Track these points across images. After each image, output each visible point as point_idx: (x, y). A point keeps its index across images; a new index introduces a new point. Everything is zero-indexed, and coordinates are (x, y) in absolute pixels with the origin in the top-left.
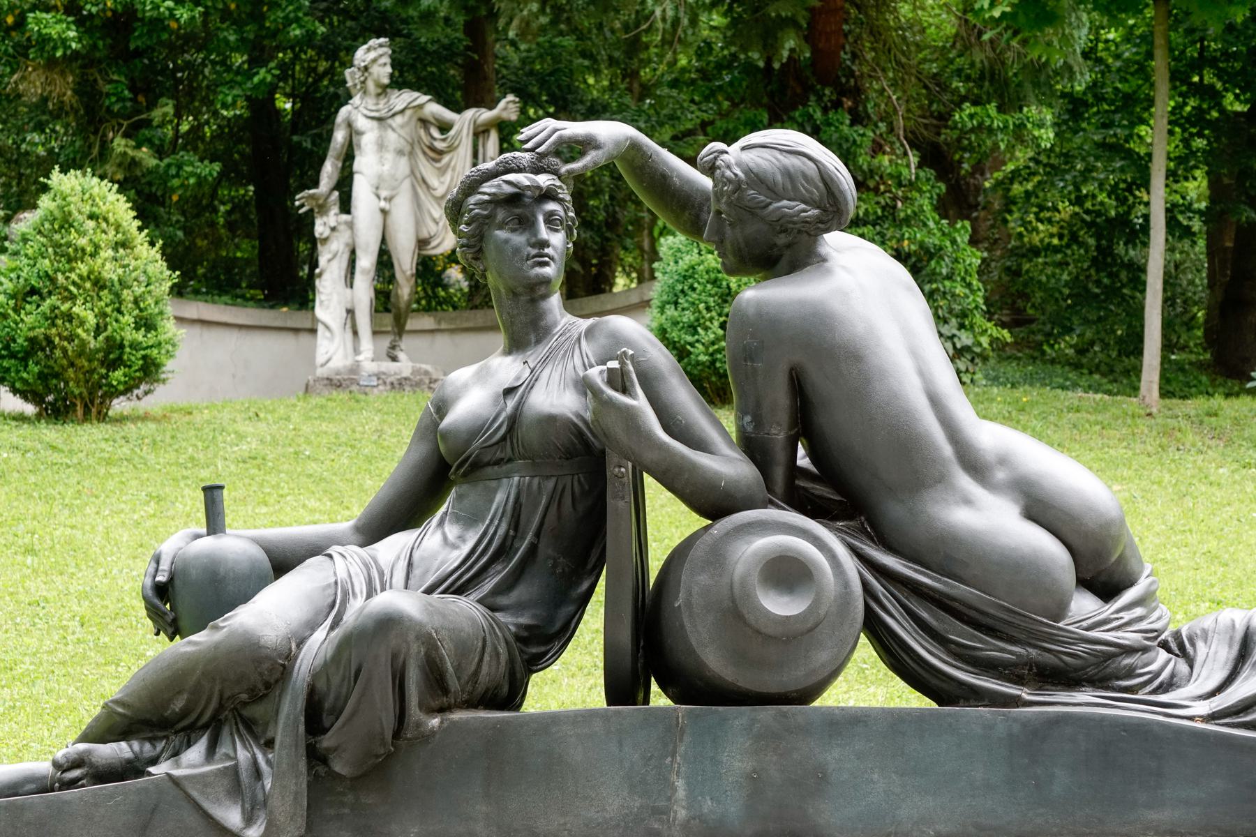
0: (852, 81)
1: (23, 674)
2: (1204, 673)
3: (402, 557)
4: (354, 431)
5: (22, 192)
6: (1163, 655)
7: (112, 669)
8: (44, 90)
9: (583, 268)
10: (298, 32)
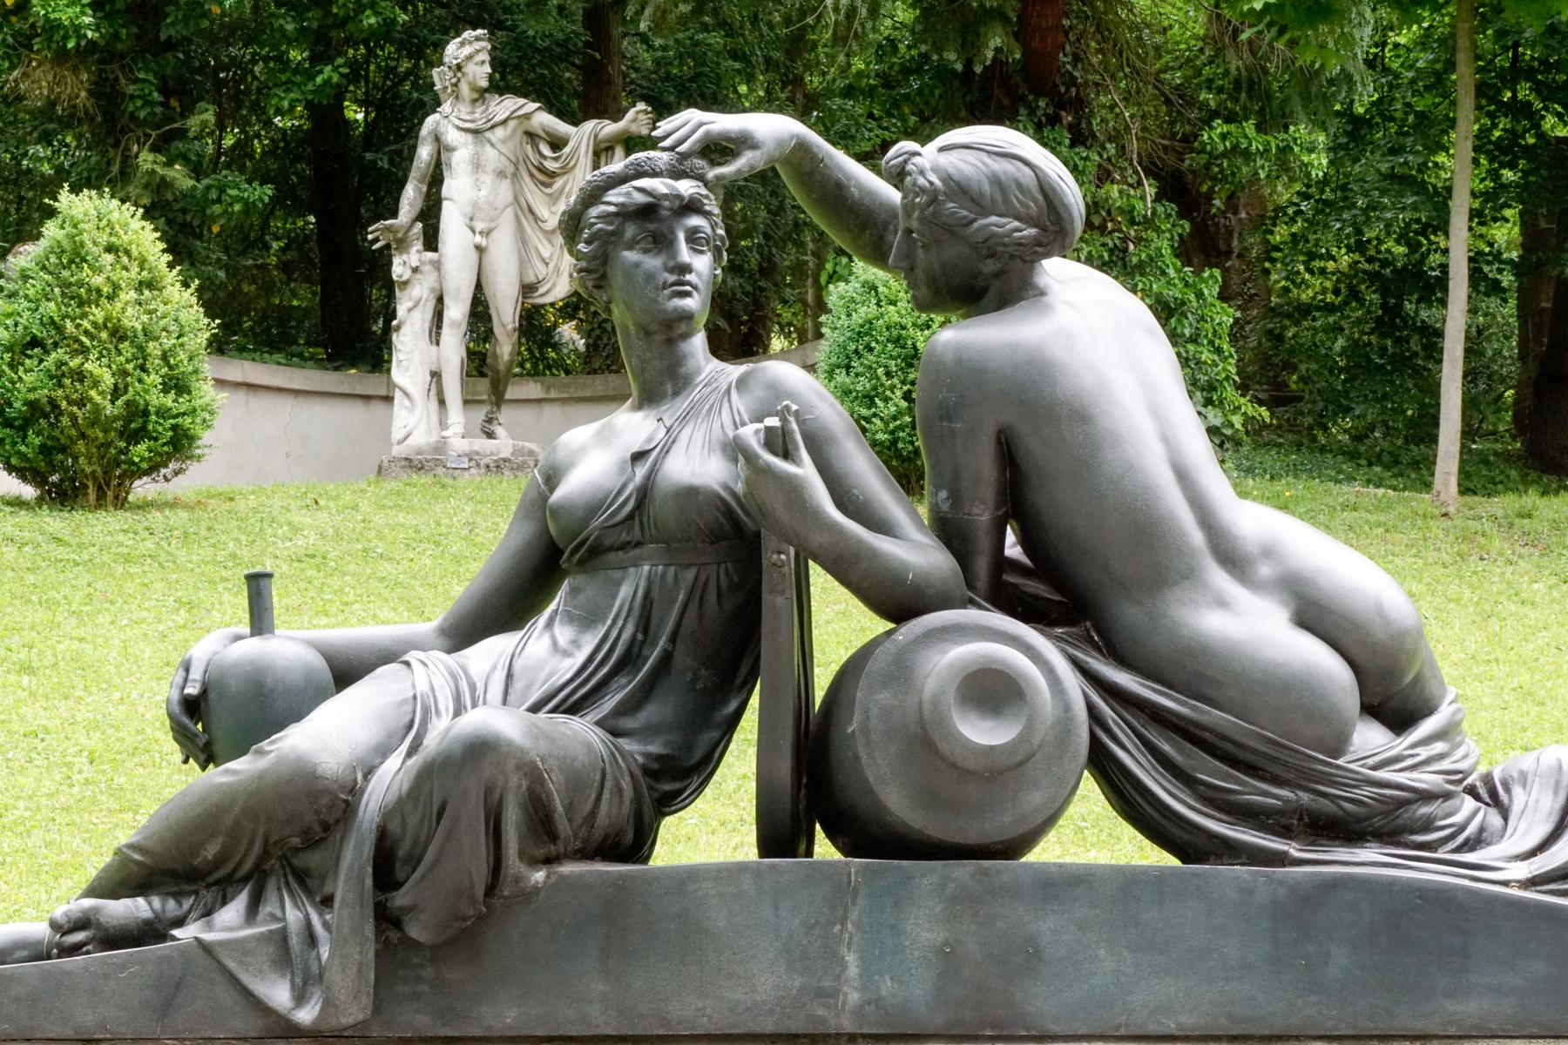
0: (1073, 90)
1: (15, 822)
2: (1522, 826)
3: (500, 666)
4: (439, 524)
5: (22, 222)
6: (1469, 803)
7: (128, 816)
8: (51, 90)
9: (731, 326)
10: (373, 20)
